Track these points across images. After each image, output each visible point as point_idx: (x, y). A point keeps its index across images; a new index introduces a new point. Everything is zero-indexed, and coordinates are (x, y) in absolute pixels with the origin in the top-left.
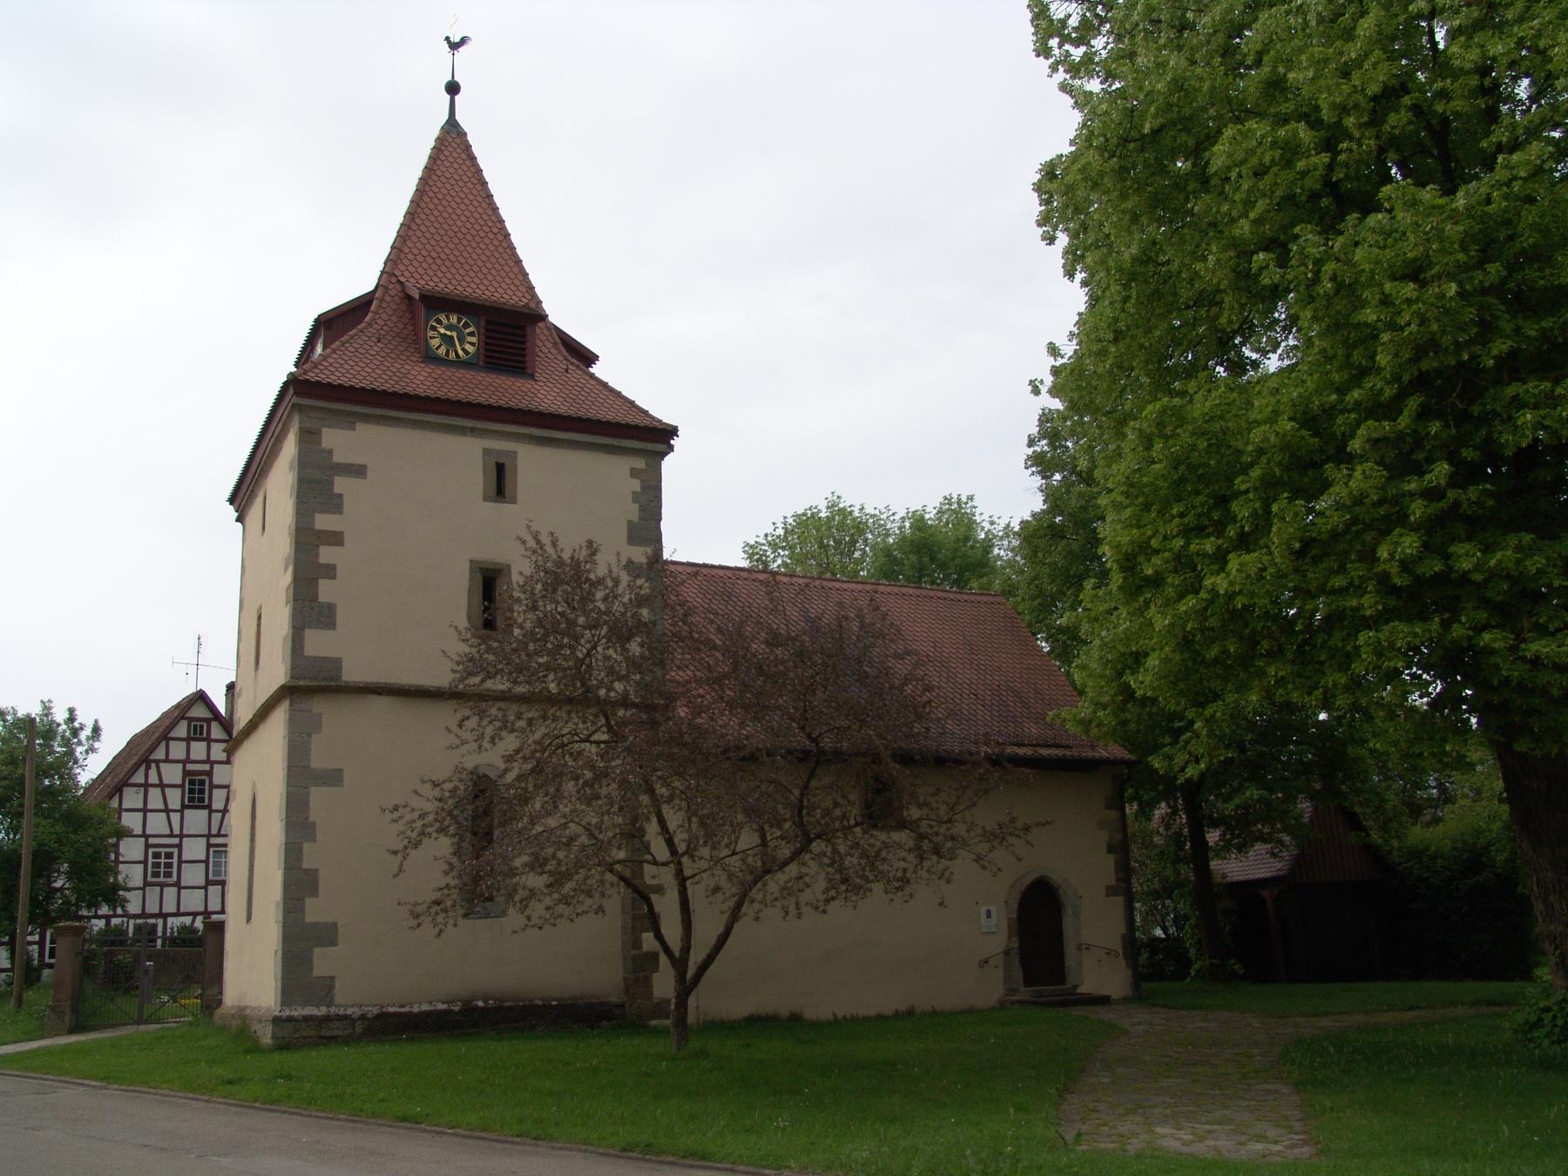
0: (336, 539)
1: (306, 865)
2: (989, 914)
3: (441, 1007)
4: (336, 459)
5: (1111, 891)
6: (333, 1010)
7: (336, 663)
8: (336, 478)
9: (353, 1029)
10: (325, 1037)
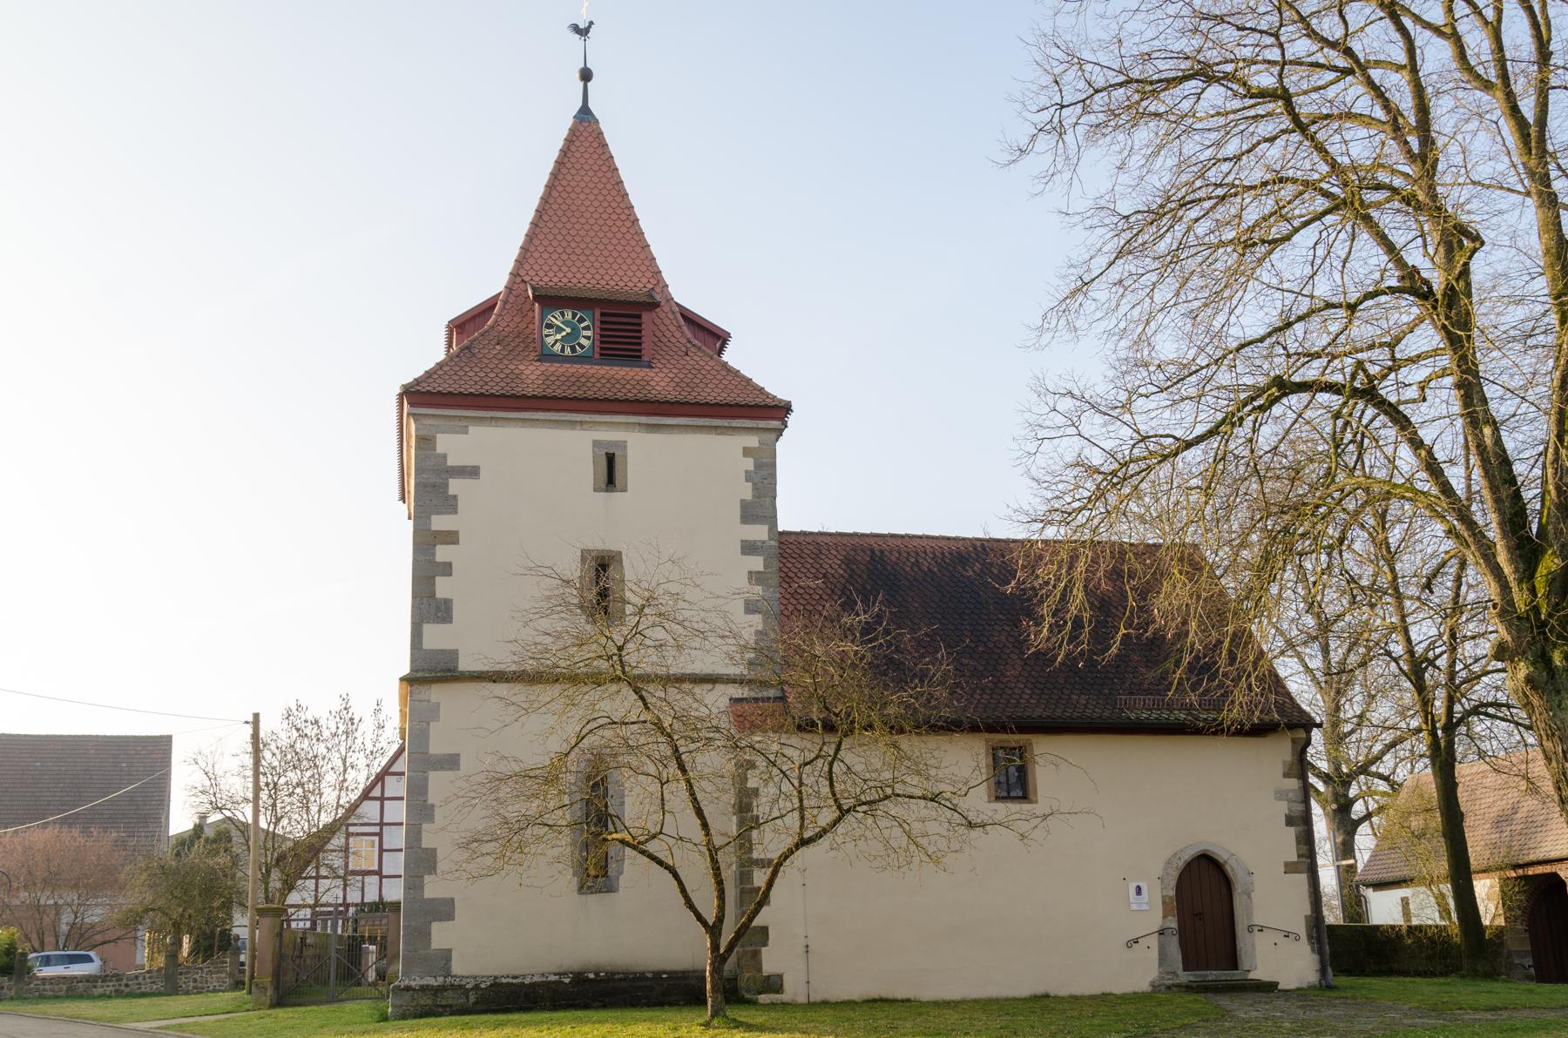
0: (451, 538)
1: (424, 845)
2: (1139, 891)
3: (553, 978)
4: (450, 463)
5: (1290, 868)
6: (449, 979)
7: (453, 654)
8: (450, 480)
9: (467, 998)
10: (441, 1006)
